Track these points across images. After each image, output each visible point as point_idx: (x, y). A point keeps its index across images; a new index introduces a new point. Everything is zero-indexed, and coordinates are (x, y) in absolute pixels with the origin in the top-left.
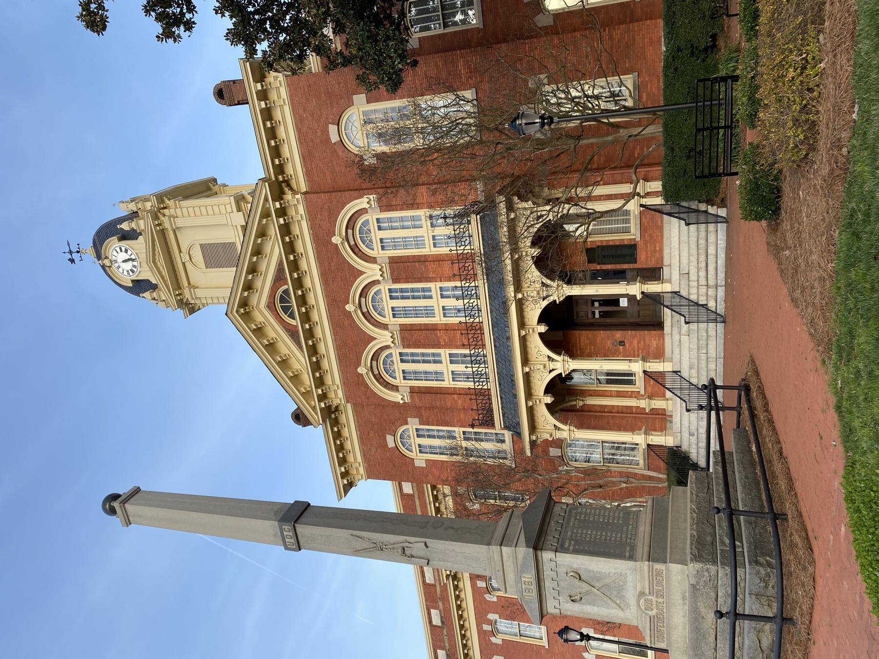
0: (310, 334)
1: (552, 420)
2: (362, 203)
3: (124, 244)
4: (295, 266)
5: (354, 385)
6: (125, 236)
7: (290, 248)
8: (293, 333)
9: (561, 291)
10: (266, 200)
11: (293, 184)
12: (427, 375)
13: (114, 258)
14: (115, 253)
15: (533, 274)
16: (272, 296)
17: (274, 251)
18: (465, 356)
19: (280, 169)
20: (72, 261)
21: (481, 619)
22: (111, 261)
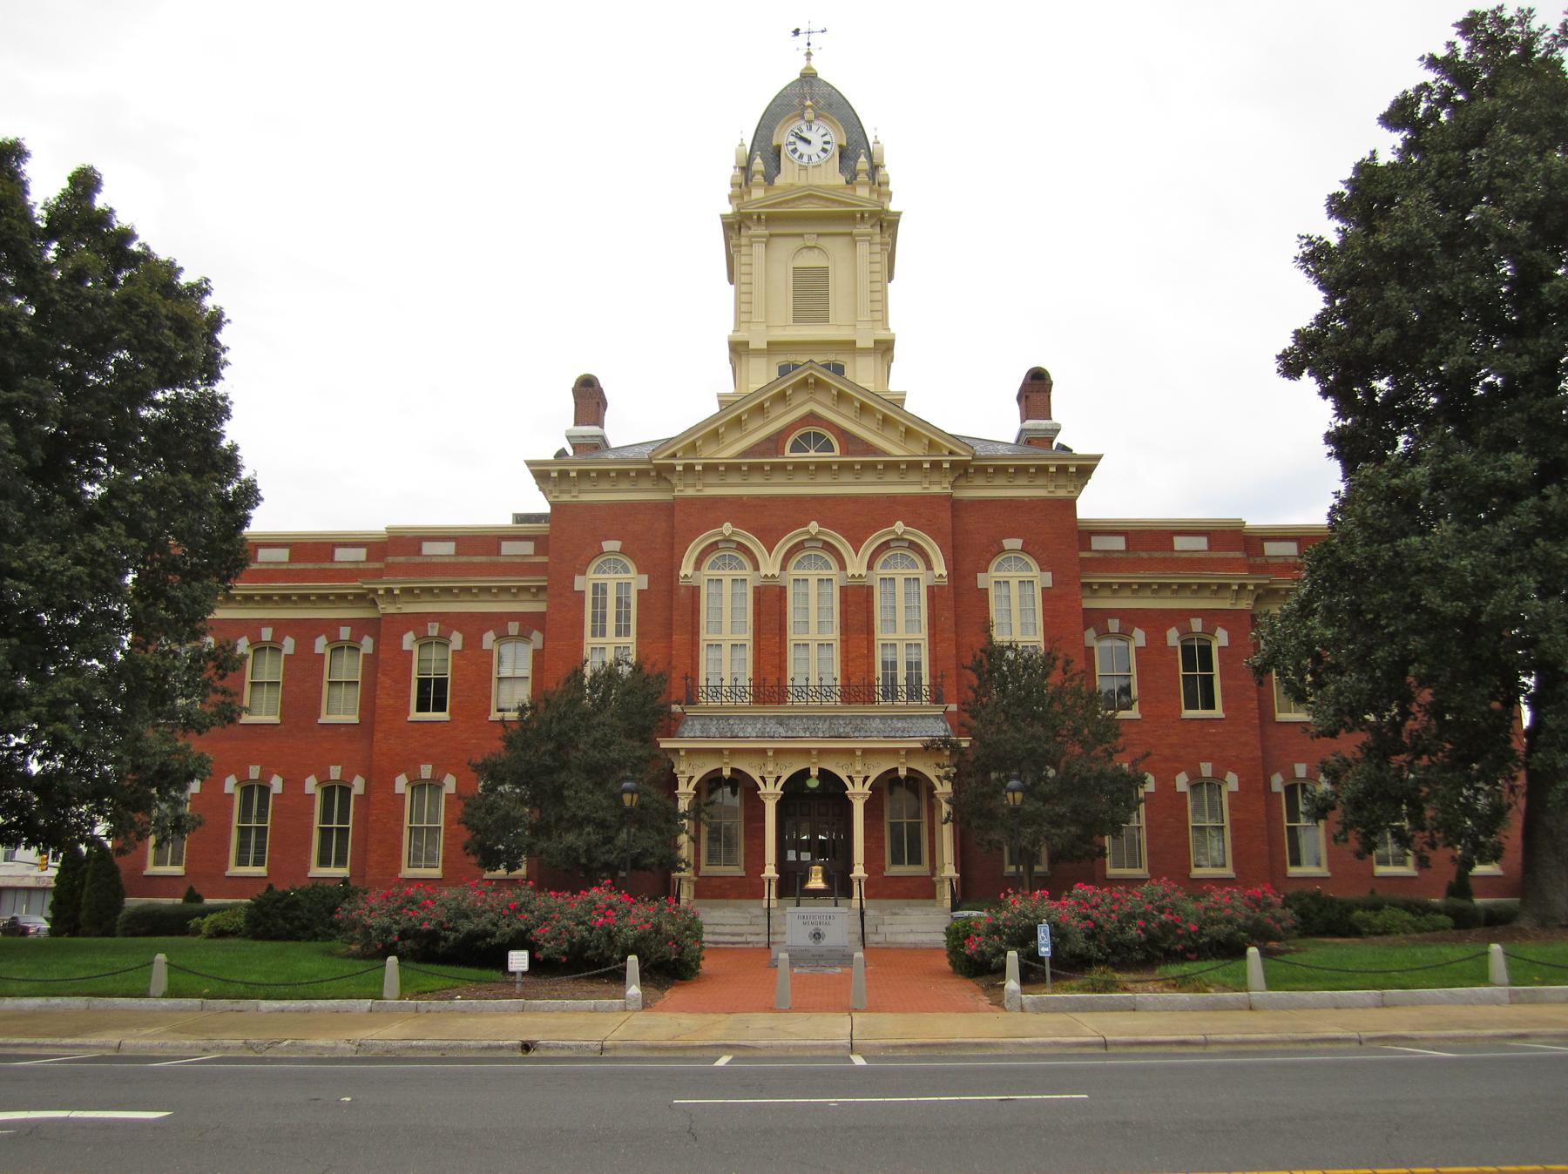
0: (754, 468)
1: (699, 775)
2: (940, 568)
3: (834, 149)
4: (869, 467)
5: (714, 510)
6: (844, 154)
7: (892, 466)
8: (774, 443)
9: (858, 793)
10: (951, 453)
11: (962, 482)
12: (600, 617)
13: (814, 127)
14: (822, 131)
15: (885, 766)
16: (830, 425)
17: (896, 449)
18: (894, 678)
19: (981, 470)
20: (796, 32)
21: (281, 627)
22: (810, 122)
